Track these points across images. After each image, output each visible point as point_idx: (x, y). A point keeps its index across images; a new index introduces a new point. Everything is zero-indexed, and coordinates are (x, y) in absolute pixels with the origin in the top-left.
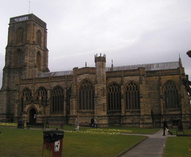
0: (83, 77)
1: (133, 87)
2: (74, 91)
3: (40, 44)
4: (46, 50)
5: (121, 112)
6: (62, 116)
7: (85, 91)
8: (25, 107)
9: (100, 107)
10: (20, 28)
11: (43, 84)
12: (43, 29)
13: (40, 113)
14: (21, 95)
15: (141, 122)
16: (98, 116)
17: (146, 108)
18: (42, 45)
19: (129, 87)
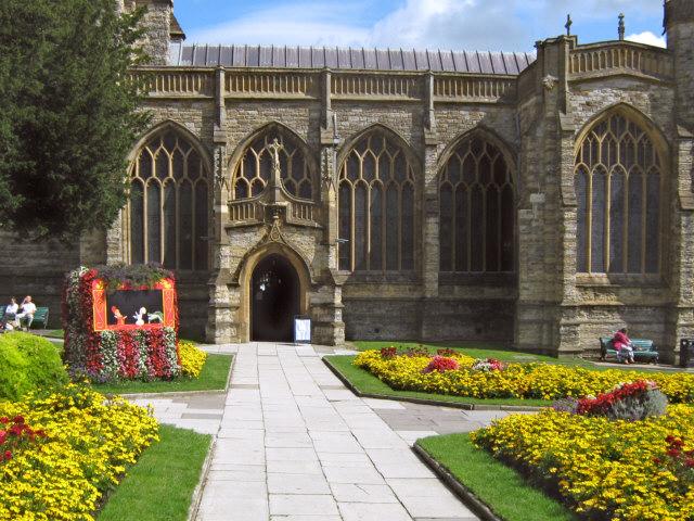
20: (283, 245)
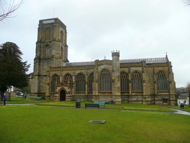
0: (102, 67)
1: (137, 75)
2: (96, 76)
3: (63, 41)
4: (66, 46)
5: (129, 93)
6: (128, 95)
7: (107, 77)
8: (57, 88)
9: (116, 89)
10: (48, 29)
12: (64, 30)
13: (69, 93)
14: (51, 79)
15: (144, 100)
16: (115, 96)
17: (147, 90)
18: (64, 42)
20: (64, 88)
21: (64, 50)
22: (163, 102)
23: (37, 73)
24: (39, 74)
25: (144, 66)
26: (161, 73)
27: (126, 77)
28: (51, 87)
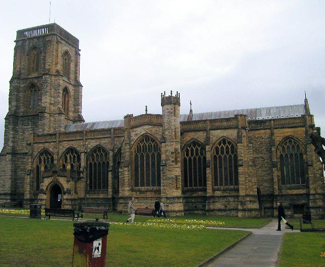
0: (141, 131)
1: (227, 147)
2: (127, 155)
4: (78, 85)
5: (205, 190)
6: (105, 197)
7: (150, 154)
8: (43, 182)
11: (73, 142)
12: (74, 49)
13: (69, 192)
14: (36, 161)
15: (240, 207)
16: (167, 198)
18: (72, 76)
19: (220, 147)
20: (57, 181)
21: (72, 93)
22: (295, 213)
23: (9, 149)
24: (13, 151)
25: (242, 128)
26: (290, 141)
27: (202, 154)
28: (35, 180)
